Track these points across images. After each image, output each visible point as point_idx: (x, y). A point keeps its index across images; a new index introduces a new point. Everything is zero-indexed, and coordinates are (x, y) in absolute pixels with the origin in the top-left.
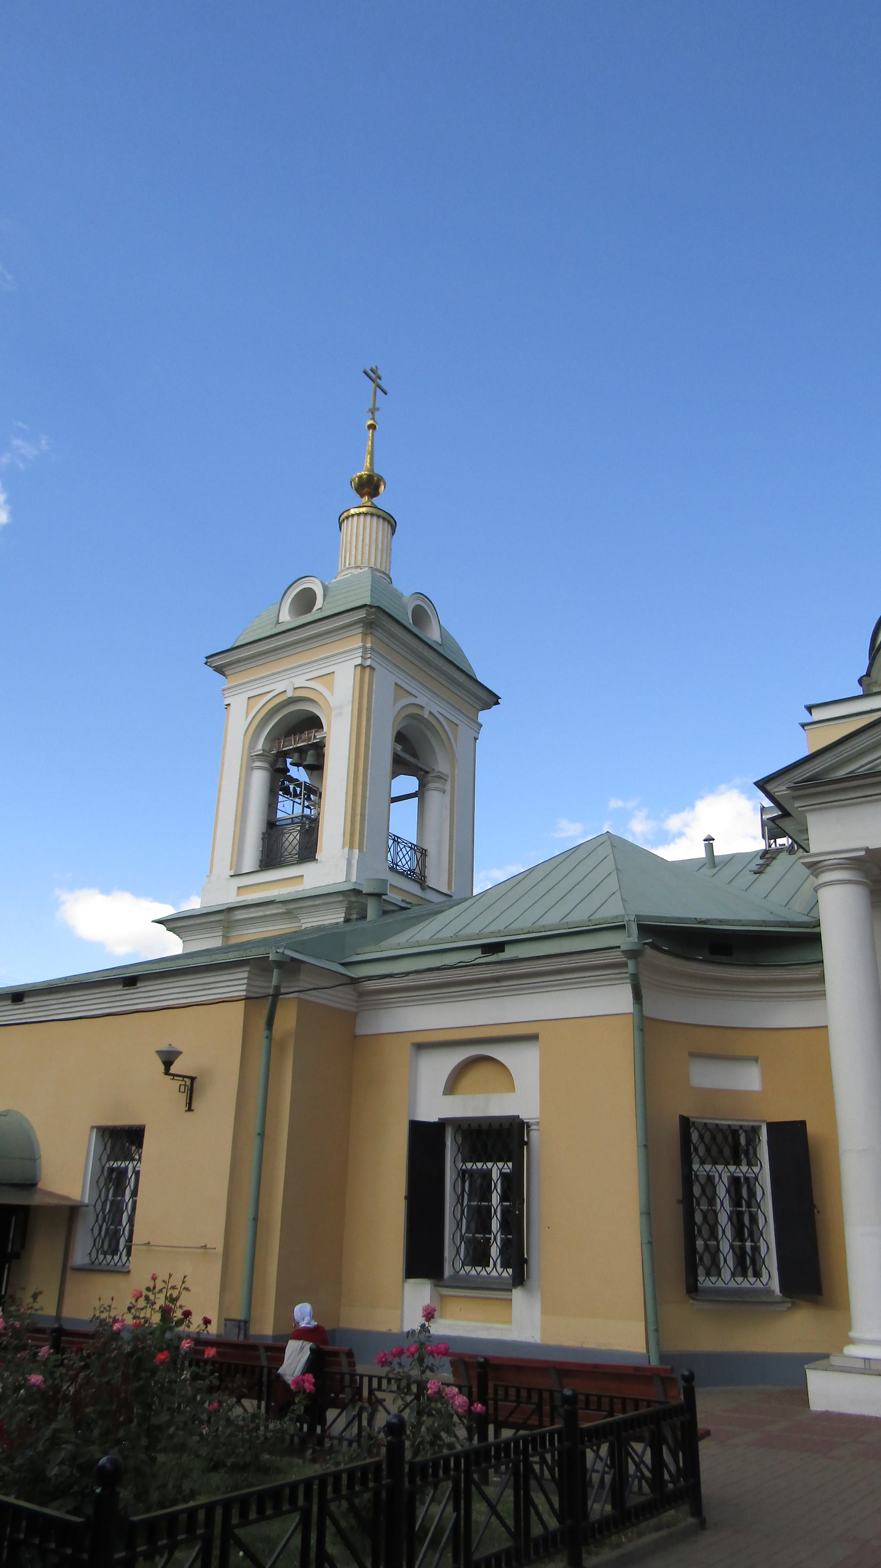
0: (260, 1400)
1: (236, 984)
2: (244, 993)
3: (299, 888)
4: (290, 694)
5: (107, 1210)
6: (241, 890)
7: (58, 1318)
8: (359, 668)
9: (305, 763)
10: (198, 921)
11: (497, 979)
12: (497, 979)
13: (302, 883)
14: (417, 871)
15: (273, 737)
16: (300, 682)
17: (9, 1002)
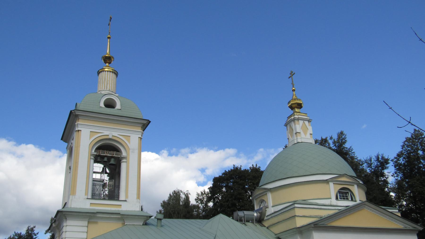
4: (110, 137)
9: (110, 163)
10: (84, 214)
15: (99, 148)
16: (116, 134)
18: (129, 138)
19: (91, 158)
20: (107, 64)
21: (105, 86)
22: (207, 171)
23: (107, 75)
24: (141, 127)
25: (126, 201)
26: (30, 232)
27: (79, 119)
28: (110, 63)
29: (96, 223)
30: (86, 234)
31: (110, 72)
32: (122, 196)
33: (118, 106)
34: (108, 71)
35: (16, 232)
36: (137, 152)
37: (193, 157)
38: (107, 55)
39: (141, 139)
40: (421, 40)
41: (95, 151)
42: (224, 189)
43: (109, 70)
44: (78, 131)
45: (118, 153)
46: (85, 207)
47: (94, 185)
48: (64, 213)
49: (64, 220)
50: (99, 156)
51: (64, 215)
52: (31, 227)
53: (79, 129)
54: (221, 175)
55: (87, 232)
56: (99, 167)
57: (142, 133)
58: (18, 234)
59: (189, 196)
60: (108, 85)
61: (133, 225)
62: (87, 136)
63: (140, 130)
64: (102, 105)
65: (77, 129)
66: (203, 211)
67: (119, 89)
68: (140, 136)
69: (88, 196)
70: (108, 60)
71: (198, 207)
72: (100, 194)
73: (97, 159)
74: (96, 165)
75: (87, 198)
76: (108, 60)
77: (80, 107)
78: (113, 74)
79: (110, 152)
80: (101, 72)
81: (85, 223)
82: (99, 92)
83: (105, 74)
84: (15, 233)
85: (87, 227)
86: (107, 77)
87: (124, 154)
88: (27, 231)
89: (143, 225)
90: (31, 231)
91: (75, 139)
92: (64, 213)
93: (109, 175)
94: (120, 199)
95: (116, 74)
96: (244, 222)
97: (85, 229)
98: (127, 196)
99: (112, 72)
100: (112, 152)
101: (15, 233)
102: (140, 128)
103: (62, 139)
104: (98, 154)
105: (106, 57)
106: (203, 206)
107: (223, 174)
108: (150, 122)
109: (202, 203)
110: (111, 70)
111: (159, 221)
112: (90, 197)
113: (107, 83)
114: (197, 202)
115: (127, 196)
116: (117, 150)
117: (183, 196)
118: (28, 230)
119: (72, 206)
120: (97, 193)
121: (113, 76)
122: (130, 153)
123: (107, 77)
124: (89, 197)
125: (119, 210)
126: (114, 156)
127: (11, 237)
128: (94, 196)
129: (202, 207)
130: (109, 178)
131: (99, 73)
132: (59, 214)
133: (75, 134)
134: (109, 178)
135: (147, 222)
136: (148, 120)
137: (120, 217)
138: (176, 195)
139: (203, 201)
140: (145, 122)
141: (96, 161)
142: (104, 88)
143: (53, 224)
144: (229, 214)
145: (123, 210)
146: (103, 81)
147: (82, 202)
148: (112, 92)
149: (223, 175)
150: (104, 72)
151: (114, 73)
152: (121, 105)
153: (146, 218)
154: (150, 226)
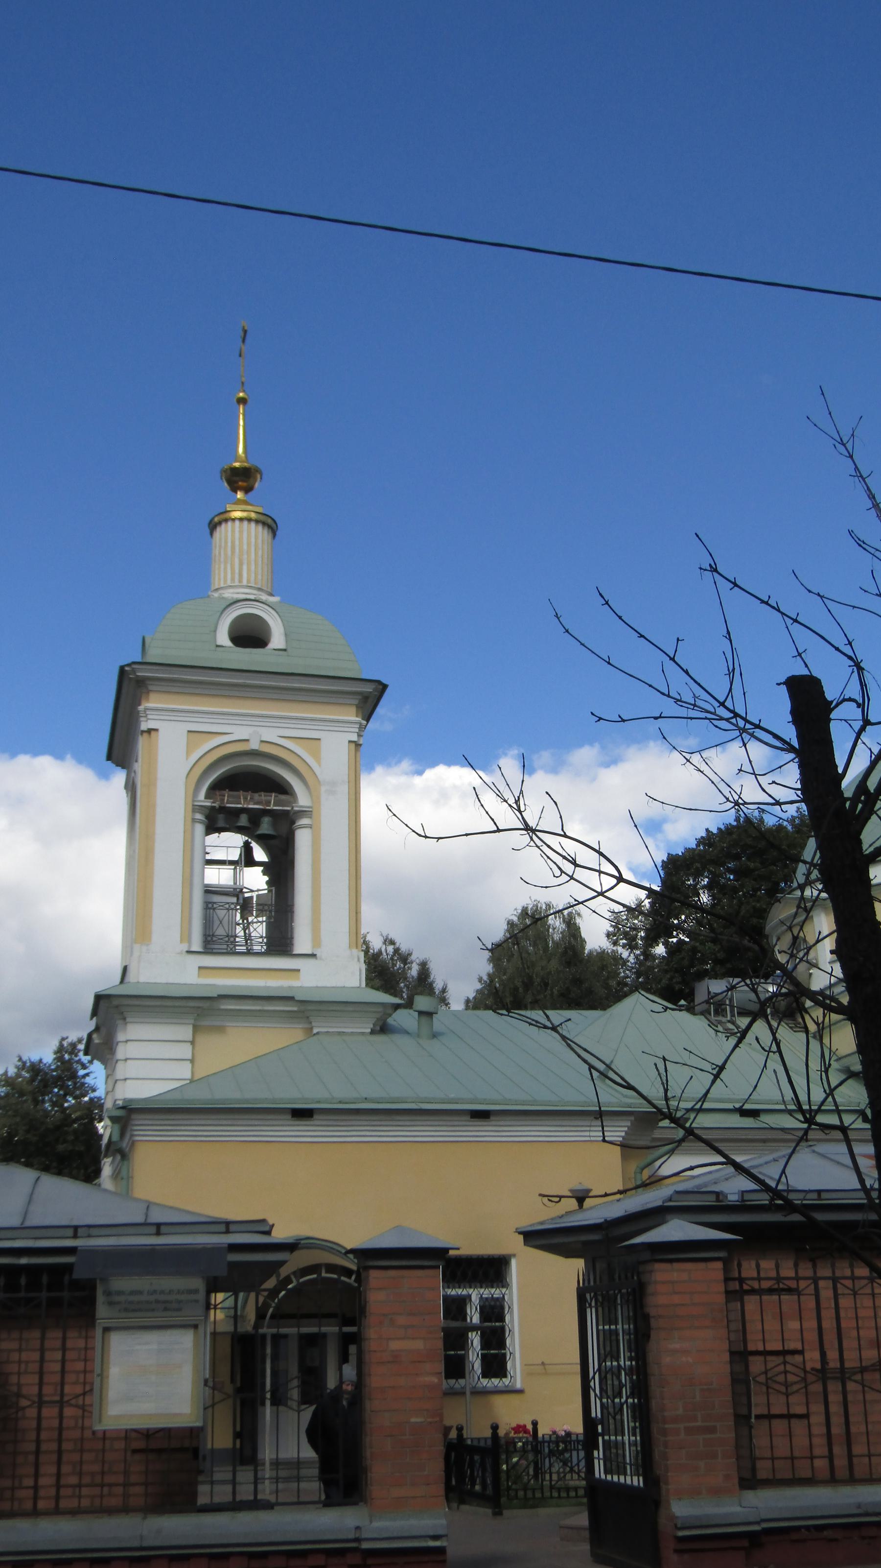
0: (212, 1450)
1: (617, 1132)
2: (621, 1139)
3: (295, 983)
4: (254, 745)
5: (619, 1297)
6: (203, 971)
7: (298, 1387)
8: (353, 746)
9: (259, 832)
10: (177, 1003)
11: (764, 1141)
12: (764, 1141)
13: (298, 978)
14: (214, 939)
15: (217, 787)
16: (270, 735)
17: (289, 1117)
18: (314, 744)
19: (194, 821)
20: (240, 495)
21: (233, 573)
22: (668, 827)
23: (241, 532)
24: (358, 707)
25: (313, 956)
26: (67, 1057)
27: (148, 692)
28: (248, 490)
29: (221, 1029)
30: (188, 1065)
31: (249, 520)
32: (302, 942)
33: (277, 640)
34: (241, 519)
35: (25, 1058)
36: (343, 790)
37: (612, 777)
38: (237, 465)
39: (357, 745)
40: (567, 631)
41: (207, 797)
42: (705, 898)
43: (244, 514)
44: (149, 731)
45: (283, 797)
46: (182, 981)
47: (209, 907)
48: (115, 1002)
49: (120, 1022)
50: (222, 809)
51: (117, 1007)
52: (70, 1040)
53: (151, 725)
54: (693, 844)
55: (192, 1061)
56: (229, 844)
57: (362, 728)
58: (33, 1065)
59: (578, 921)
60: (245, 567)
61: (339, 1033)
62: (181, 742)
63: (351, 715)
64: (223, 638)
65: (144, 726)
66: (638, 974)
67: (281, 579)
68: (354, 737)
69: (190, 942)
70: (241, 478)
71: (617, 959)
72: (231, 938)
73: (216, 821)
74: (213, 839)
75: (189, 952)
76: (241, 478)
77: (155, 654)
78: (260, 527)
79: (256, 796)
80: (220, 523)
81: (185, 1032)
82: (216, 595)
83: (233, 531)
84: (20, 1059)
85: (192, 1043)
86: (241, 539)
87: (303, 800)
88: (56, 1053)
89: (373, 1032)
90: (71, 1053)
91: (140, 760)
92: (115, 1002)
93: (267, 868)
94: (296, 952)
95: (269, 527)
96: (733, 1015)
97: (186, 1051)
98: (316, 940)
99: (257, 521)
100: (263, 797)
101: (20, 1059)
102: (353, 710)
103: (109, 758)
104: (216, 805)
105: (234, 470)
106: (637, 957)
107: (701, 841)
108: (385, 687)
109: (631, 946)
110: (253, 515)
111: (424, 1019)
112: (197, 946)
113: (240, 559)
114: (615, 943)
115: (316, 940)
116: (282, 788)
117: (556, 923)
118: (60, 1050)
119: (142, 979)
120: (220, 932)
121: (257, 533)
122: (324, 797)
123: (241, 539)
124: (194, 949)
125: (291, 988)
126: (272, 807)
127: (6, 1073)
128: (213, 942)
129: (632, 959)
130: (266, 878)
131: (213, 526)
132: (102, 1004)
133: (142, 742)
134: (266, 878)
135: (390, 1021)
136: (379, 682)
137: (295, 1009)
138: (532, 922)
139: (634, 938)
140: (368, 689)
141: (212, 828)
142: (233, 580)
143: (95, 1036)
144: (495, 1011)
145: (307, 984)
146: (226, 555)
147: (174, 965)
148: (260, 589)
149: (698, 845)
150: (230, 523)
151: (264, 524)
152: (286, 635)
153: (380, 1009)
154: (396, 1037)
